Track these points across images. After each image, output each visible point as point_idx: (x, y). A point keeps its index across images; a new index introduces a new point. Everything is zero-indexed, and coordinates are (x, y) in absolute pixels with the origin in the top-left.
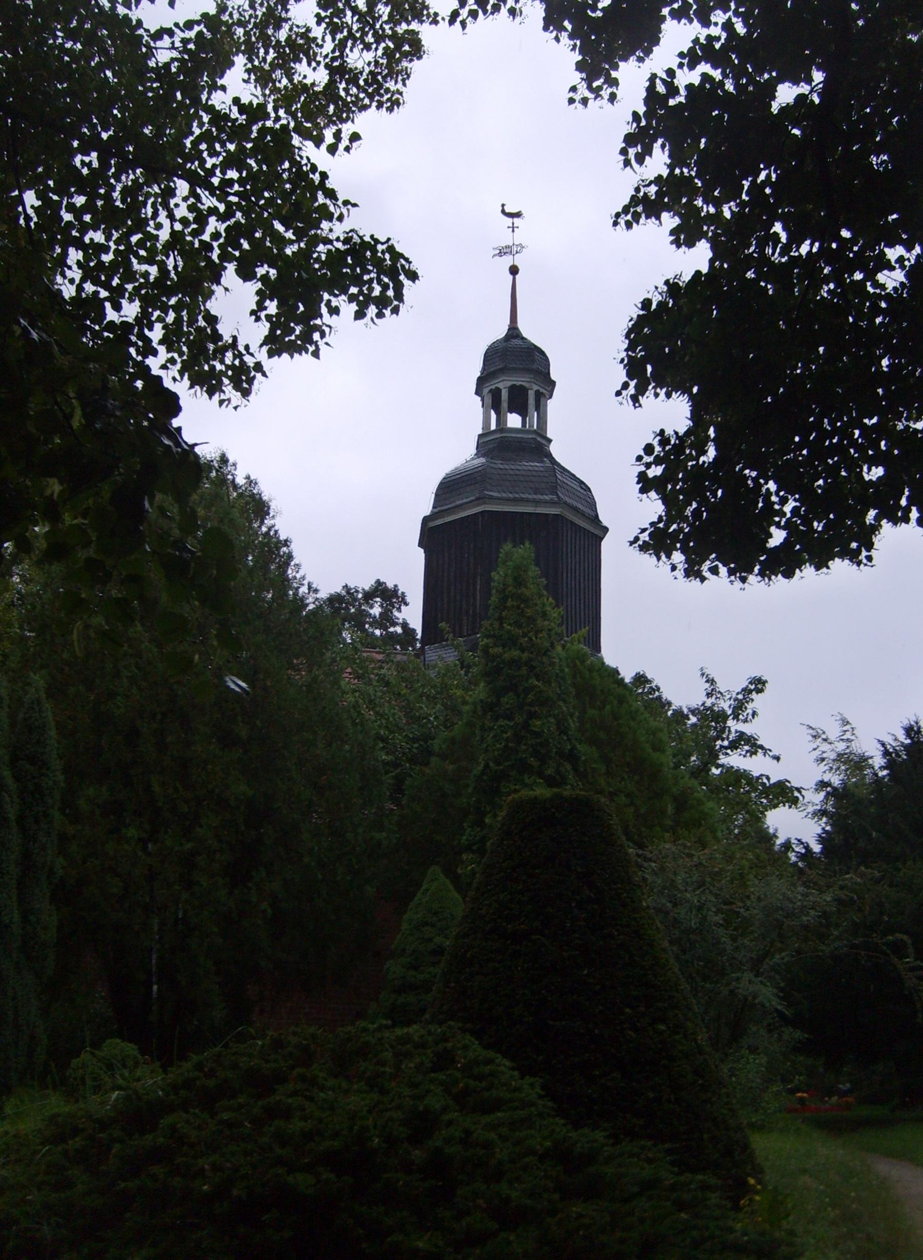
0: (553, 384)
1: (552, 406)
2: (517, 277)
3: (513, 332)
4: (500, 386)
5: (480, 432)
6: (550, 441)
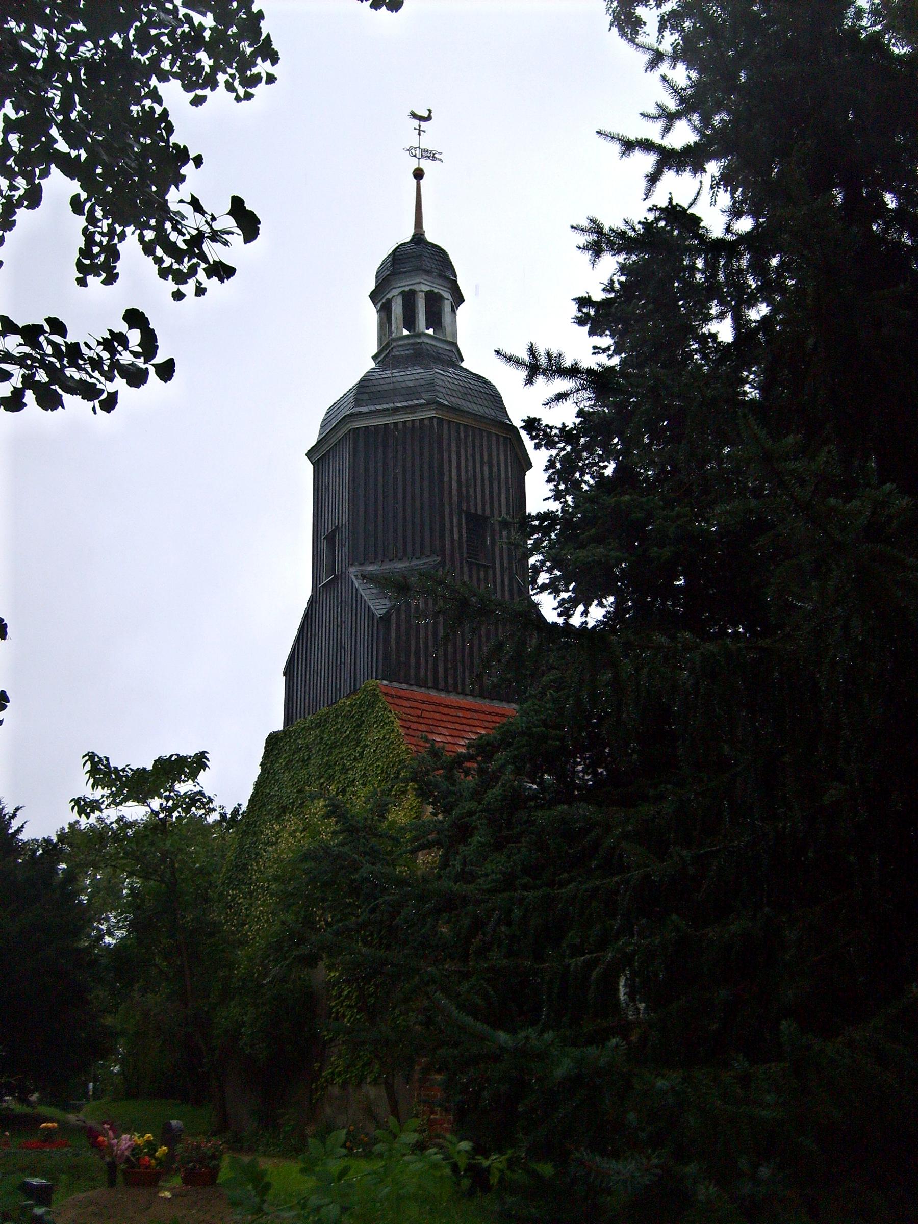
2: (421, 181)
3: (419, 238)
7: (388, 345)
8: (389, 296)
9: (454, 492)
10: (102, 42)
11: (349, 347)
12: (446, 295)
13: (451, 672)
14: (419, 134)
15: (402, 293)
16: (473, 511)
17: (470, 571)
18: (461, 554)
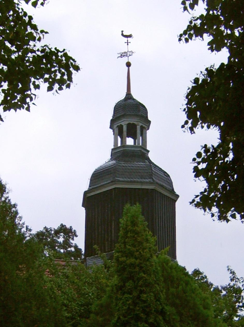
0: (149, 122)
1: (150, 134)
2: (130, 68)
3: (129, 96)
4: (122, 124)
5: (113, 147)
6: (148, 151)
10: (51, 80)
11: (99, 147)
14: (128, 44)
15: (118, 126)
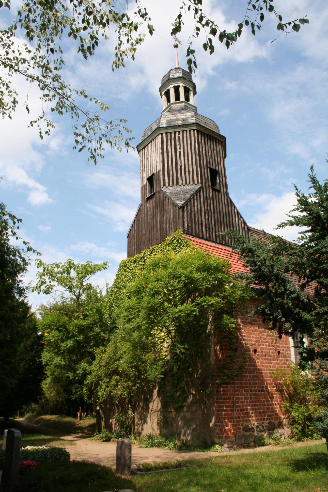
7: (169, 106)
8: (169, 88)
9: (205, 160)
12: (191, 89)
13: (208, 232)
16: (214, 168)
17: (213, 192)
18: (209, 185)
